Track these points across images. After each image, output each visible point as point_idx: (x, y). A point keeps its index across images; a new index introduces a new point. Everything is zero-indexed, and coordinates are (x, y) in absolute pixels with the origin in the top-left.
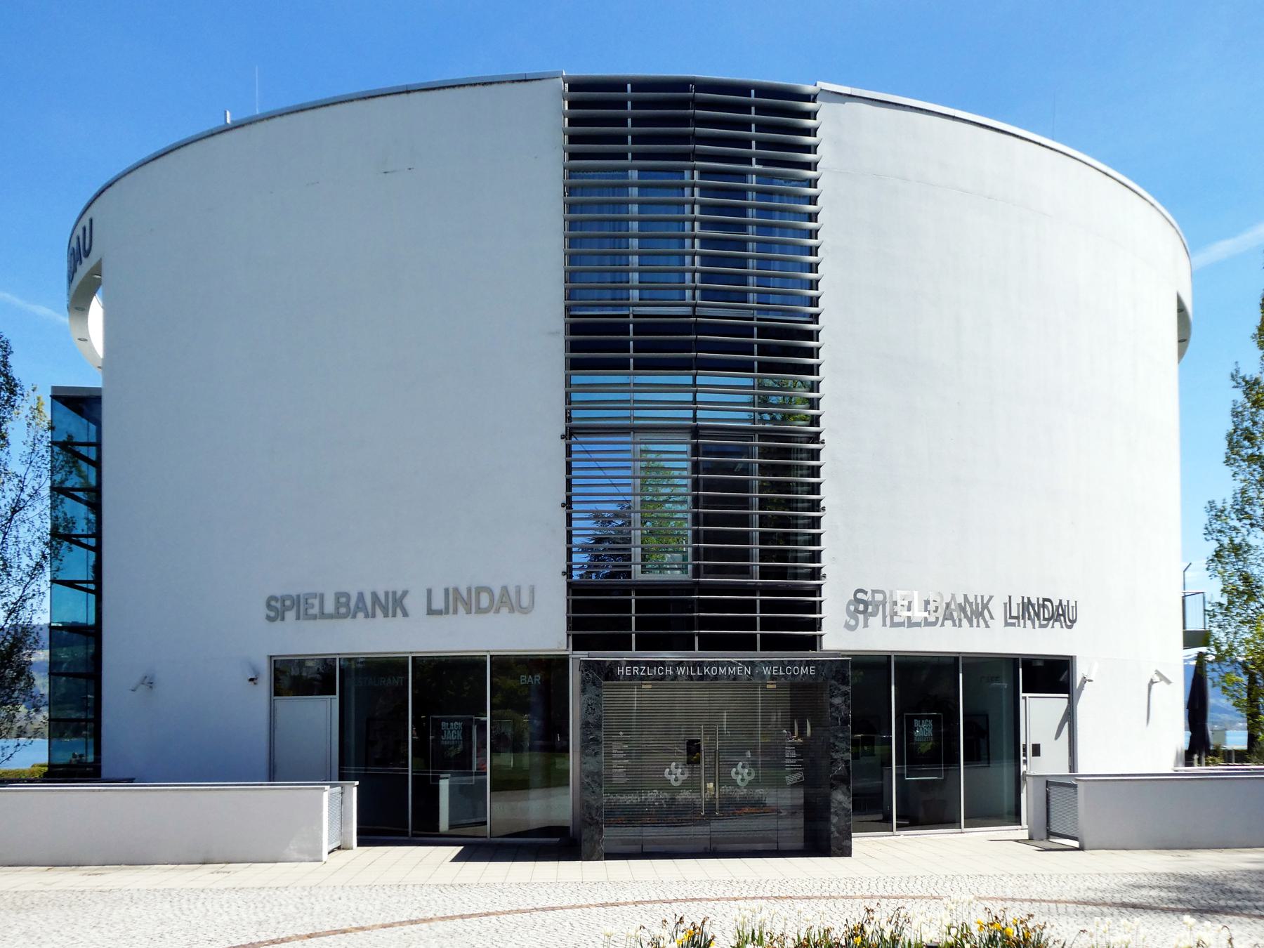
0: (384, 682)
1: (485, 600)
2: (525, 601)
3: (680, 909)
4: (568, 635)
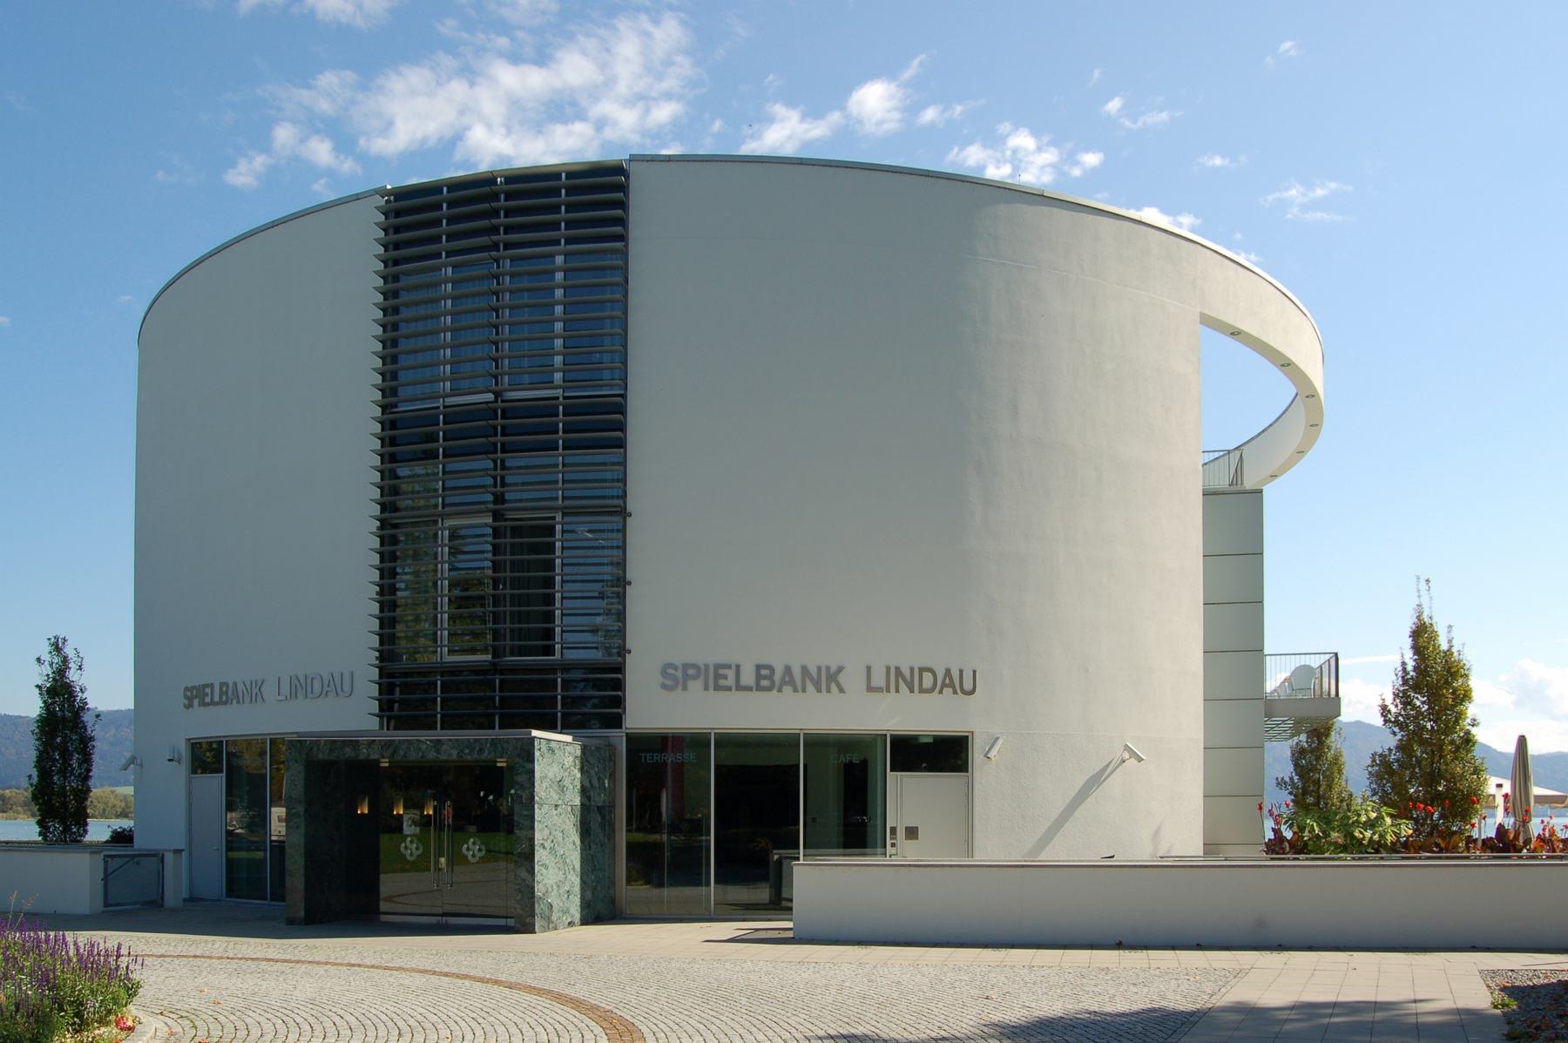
0: (658, 758)
1: (928, 680)
2: (968, 686)
3: (956, 963)
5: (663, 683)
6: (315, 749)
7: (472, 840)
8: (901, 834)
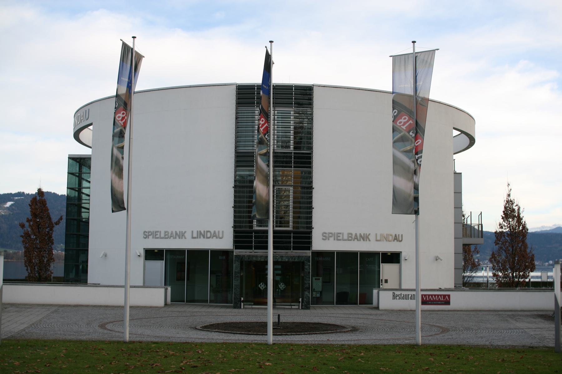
2: (221, 236)
4: (233, 245)
5: (323, 238)
6: (244, 258)
7: (261, 283)
8: (384, 281)
